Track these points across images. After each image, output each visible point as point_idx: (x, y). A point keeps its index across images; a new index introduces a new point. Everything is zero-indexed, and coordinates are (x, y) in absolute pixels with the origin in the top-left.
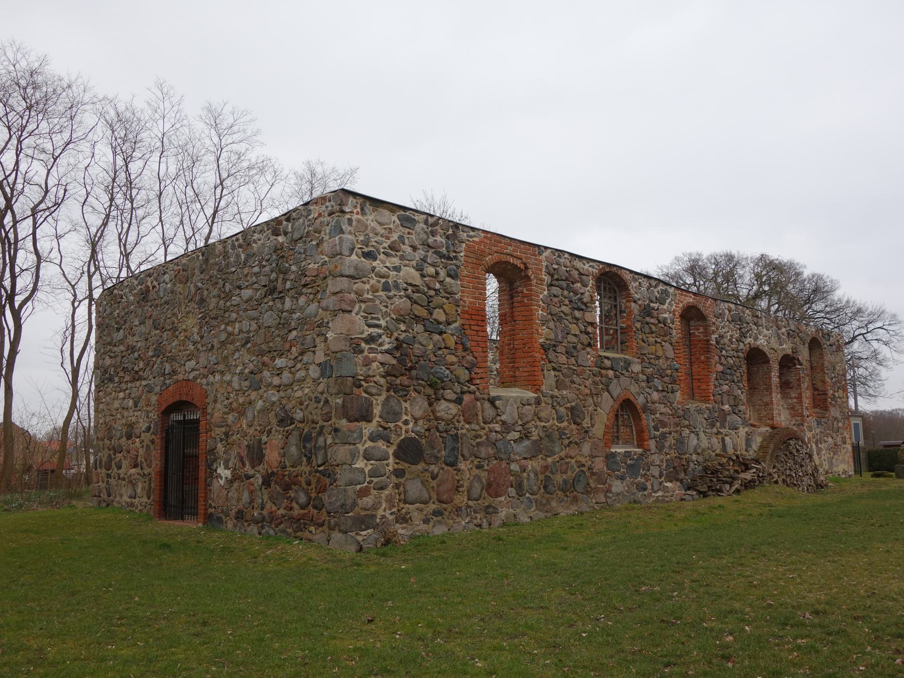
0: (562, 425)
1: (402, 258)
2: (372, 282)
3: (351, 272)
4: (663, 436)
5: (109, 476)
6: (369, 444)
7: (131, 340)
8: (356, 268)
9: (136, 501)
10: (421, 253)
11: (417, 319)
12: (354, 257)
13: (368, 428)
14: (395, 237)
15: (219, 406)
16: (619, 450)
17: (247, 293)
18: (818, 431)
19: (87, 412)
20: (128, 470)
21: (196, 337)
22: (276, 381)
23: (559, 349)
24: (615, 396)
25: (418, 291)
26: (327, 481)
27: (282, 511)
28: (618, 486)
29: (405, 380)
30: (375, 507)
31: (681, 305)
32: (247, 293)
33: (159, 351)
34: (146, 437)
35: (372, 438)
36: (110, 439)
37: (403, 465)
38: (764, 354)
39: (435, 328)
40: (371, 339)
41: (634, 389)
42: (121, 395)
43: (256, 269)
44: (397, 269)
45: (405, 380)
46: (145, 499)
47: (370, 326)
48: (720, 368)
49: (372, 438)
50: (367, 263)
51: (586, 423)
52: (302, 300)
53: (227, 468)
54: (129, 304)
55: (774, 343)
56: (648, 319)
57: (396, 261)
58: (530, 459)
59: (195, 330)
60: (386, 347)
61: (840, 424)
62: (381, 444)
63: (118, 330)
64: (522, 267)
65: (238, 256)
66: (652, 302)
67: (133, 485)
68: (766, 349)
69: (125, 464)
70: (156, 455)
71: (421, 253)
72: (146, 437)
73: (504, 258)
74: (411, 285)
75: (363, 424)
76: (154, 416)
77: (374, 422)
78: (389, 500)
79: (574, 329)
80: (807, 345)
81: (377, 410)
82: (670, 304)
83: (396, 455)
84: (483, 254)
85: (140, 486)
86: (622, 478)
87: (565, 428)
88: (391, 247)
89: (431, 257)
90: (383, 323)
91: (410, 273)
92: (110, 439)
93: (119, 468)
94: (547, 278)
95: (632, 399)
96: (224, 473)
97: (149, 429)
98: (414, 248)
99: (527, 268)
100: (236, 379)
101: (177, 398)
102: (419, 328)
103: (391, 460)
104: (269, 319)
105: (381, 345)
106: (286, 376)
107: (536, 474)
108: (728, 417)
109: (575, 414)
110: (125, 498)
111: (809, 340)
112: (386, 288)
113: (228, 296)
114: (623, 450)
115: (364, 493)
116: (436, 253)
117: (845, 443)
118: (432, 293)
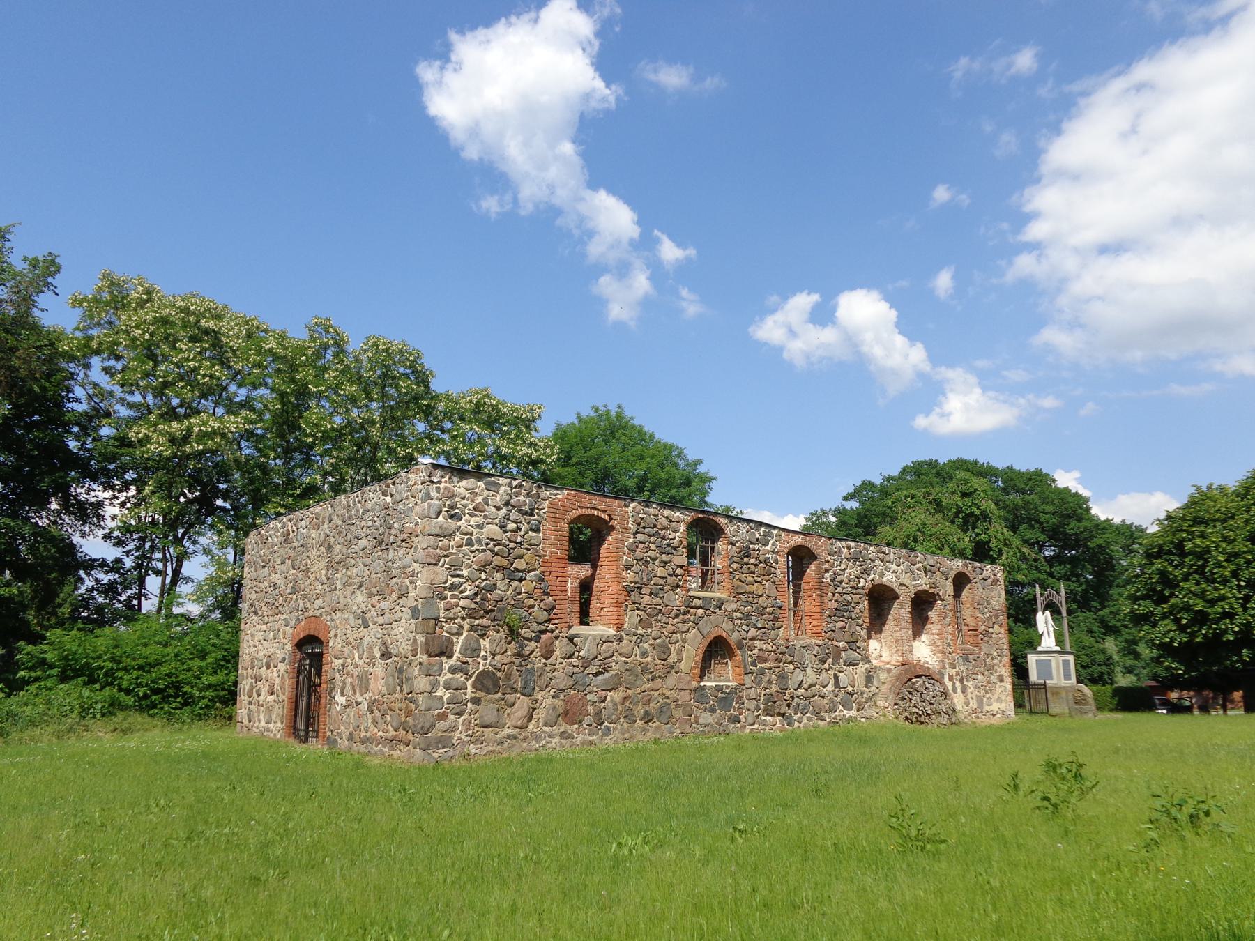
0: (645, 660)
1: (486, 517)
2: (420, 554)
3: (437, 531)
4: (762, 672)
5: (250, 703)
6: (450, 676)
7: (274, 578)
8: (441, 528)
9: (271, 726)
10: (504, 511)
11: (498, 568)
12: (441, 518)
13: (447, 664)
14: (479, 499)
15: (338, 640)
16: (708, 684)
17: (363, 543)
18: (964, 668)
19: (1036, 65)
20: (265, 697)
21: (324, 579)
22: (381, 620)
23: (643, 591)
24: (705, 632)
25: (499, 545)
26: (413, 707)
27: (381, 734)
28: (706, 718)
29: (484, 622)
30: (452, 729)
31: (787, 545)
32: (363, 543)
33: (295, 590)
34: (282, 667)
35: (453, 670)
36: (253, 668)
37: (479, 694)
38: (893, 590)
39: (513, 575)
40: (453, 587)
41: (727, 626)
42: (264, 627)
43: (370, 523)
44: (480, 527)
45: (484, 622)
46: (279, 724)
47: (453, 576)
48: (834, 605)
49: (453, 670)
50: (452, 523)
51: (673, 658)
52: (402, 552)
53: (343, 695)
54: (274, 544)
55: (906, 579)
56: (746, 559)
57: (480, 520)
58: (610, 691)
59: (324, 572)
60: (468, 593)
61: (995, 661)
62: (459, 676)
63: (264, 567)
64: (607, 518)
65: (357, 510)
66: (752, 543)
67: (269, 710)
68: (894, 586)
69: (264, 692)
70: (289, 683)
71: (504, 511)
72: (282, 667)
73: (581, 512)
74: (492, 540)
75: (444, 659)
76: (289, 647)
77: (455, 658)
78: (467, 725)
79: (661, 572)
80: (951, 580)
81: (457, 648)
82: (774, 544)
83: (473, 686)
84: (566, 509)
85: (276, 711)
86: (713, 711)
87: (647, 663)
88: (475, 509)
89: (514, 515)
90: (465, 573)
91: (492, 530)
92: (253, 668)
93: (259, 695)
94: (633, 527)
95: (724, 635)
96: (341, 700)
97: (284, 659)
98: (498, 509)
99: (611, 519)
100: (352, 617)
101: (307, 633)
102: (498, 576)
103: (470, 689)
104: (377, 566)
105: (462, 592)
106: (388, 617)
107: (615, 705)
108: (843, 654)
109: (664, 651)
110: (263, 723)
111: (953, 574)
112: (470, 543)
113: (349, 544)
114: (714, 684)
115: (442, 717)
116: (520, 511)
117: (1002, 681)
118: (512, 545)
